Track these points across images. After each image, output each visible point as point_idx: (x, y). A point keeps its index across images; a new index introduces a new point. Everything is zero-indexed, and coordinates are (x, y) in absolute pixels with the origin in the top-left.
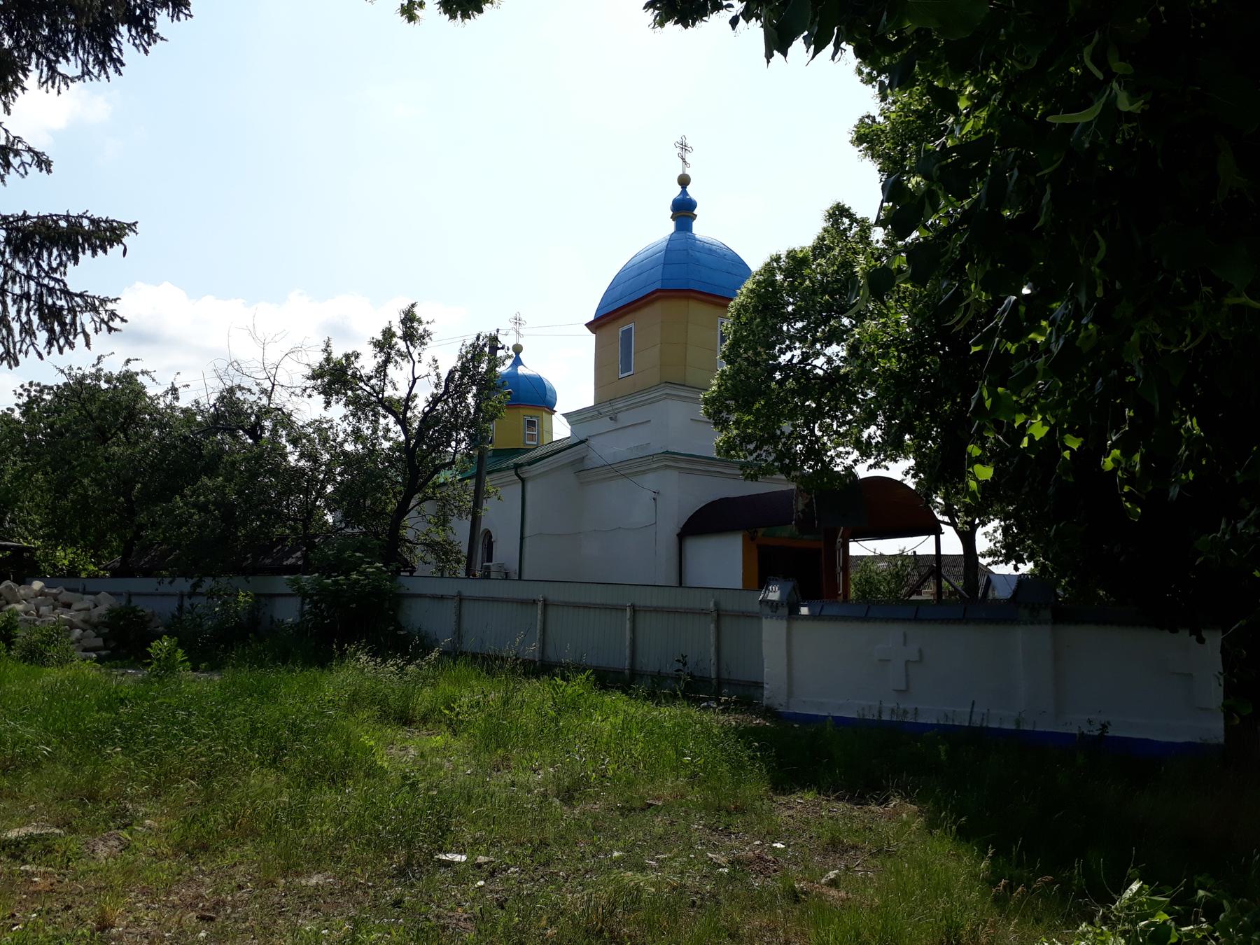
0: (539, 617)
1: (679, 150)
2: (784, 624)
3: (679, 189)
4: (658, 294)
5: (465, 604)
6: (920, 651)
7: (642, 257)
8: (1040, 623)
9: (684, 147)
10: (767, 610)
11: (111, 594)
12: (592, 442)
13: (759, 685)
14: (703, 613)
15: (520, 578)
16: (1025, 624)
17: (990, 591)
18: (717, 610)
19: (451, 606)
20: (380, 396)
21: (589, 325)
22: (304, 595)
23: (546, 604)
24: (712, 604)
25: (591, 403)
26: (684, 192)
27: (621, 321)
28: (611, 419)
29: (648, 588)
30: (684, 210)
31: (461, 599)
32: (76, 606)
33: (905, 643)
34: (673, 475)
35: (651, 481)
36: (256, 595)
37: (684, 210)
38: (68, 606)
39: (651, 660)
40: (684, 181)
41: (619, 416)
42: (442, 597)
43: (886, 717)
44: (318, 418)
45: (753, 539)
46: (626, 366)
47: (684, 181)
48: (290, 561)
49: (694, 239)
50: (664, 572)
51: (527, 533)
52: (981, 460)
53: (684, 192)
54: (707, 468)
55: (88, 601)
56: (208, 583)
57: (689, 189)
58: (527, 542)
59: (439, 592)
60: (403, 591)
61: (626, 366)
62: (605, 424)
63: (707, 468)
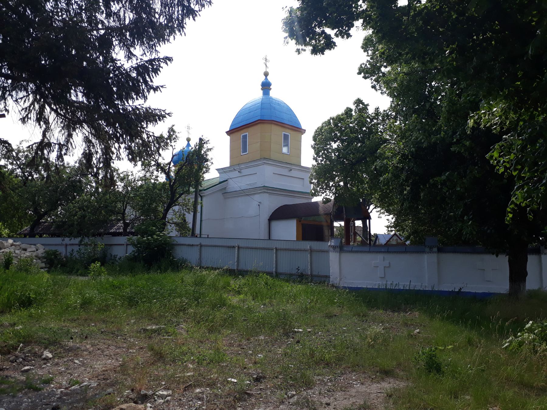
0: (236, 253)
1: (265, 61)
2: (338, 254)
3: (264, 77)
4: (259, 121)
5: (203, 248)
6: (389, 263)
7: (250, 105)
8: (433, 253)
9: (266, 60)
10: (332, 249)
11: (42, 245)
12: (230, 181)
13: (328, 277)
14: (305, 250)
15: (200, 237)
16: (428, 253)
17: (377, 241)
18: (310, 249)
19: (197, 249)
20: (143, 159)
21: (227, 132)
22: (133, 244)
23: (239, 248)
24: (309, 247)
25: (228, 165)
26: (266, 78)
27: (242, 131)
28: (239, 172)
29: (243, 240)
30: (266, 86)
31: (201, 246)
32: (29, 250)
33: (384, 260)
34: (266, 195)
35: (257, 198)
36: (105, 245)
37: (266, 86)
38: (25, 250)
39: (284, 268)
40: (266, 74)
41: (242, 171)
42: (193, 245)
43: (388, 287)
44: (126, 171)
45: (300, 221)
46: (245, 150)
47: (266, 74)
48: (112, 231)
49: (271, 98)
50: (263, 234)
51: (203, 218)
52: (510, 212)
53: (266, 78)
54: (302, 196)
55: (33, 248)
56: (86, 240)
57: (268, 77)
58: (203, 223)
59: (254, 246)
60: (175, 243)
61: (245, 150)
62: (236, 174)
63: (302, 196)
